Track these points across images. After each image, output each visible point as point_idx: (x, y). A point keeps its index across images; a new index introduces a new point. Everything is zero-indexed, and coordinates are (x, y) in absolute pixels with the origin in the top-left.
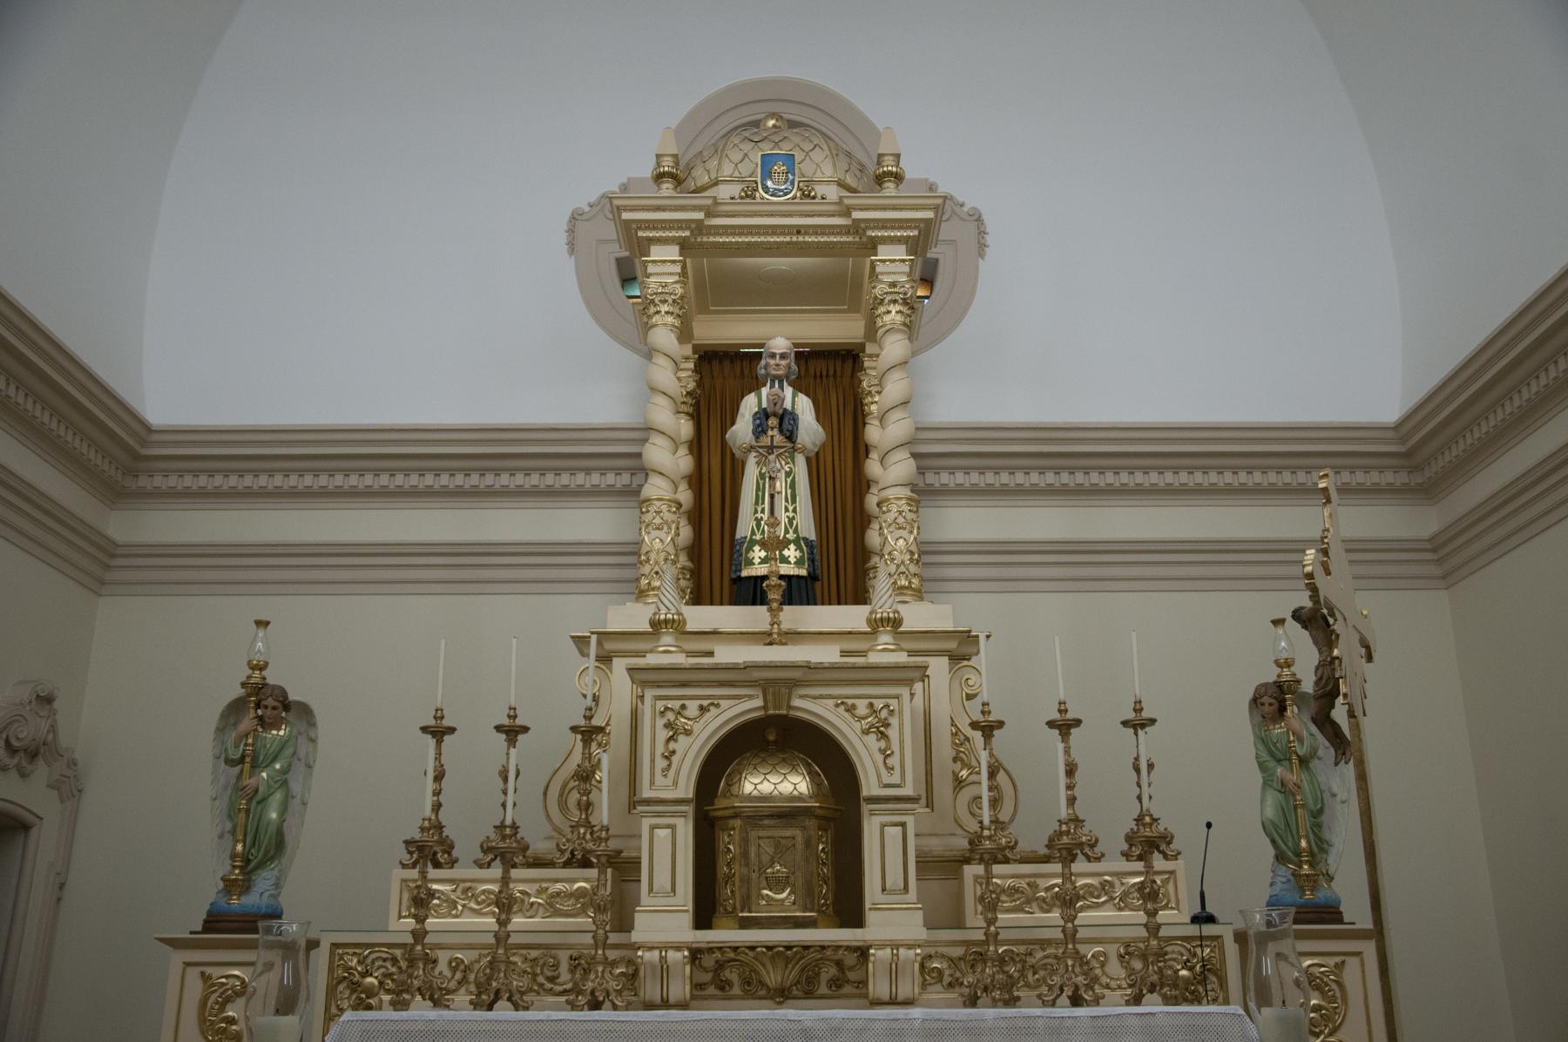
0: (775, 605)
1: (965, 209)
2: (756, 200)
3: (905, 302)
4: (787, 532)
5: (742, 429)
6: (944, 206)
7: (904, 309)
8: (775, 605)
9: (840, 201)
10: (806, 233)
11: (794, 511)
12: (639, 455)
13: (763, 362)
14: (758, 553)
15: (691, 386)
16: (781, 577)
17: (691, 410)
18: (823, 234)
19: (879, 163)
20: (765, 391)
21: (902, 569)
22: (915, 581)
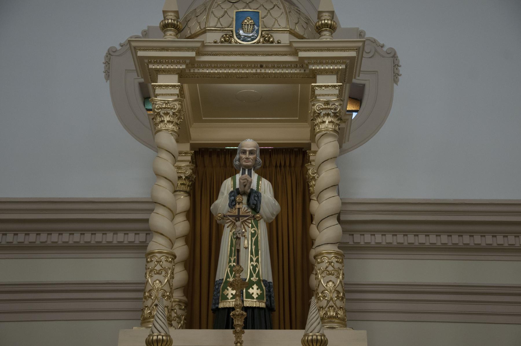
0: (238, 329)
1: (385, 49)
2: (234, 45)
3: (335, 115)
4: (251, 276)
5: (222, 203)
6: (364, 46)
7: (335, 120)
8: (238, 329)
9: (290, 45)
10: (267, 67)
11: (257, 261)
12: (147, 221)
13: (237, 157)
14: (231, 292)
15: (189, 172)
16: (246, 309)
17: (188, 189)
18: (279, 68)
19: (319, 18)
20: (238, 176)
21: (331, 303)
22: (341, 313)
